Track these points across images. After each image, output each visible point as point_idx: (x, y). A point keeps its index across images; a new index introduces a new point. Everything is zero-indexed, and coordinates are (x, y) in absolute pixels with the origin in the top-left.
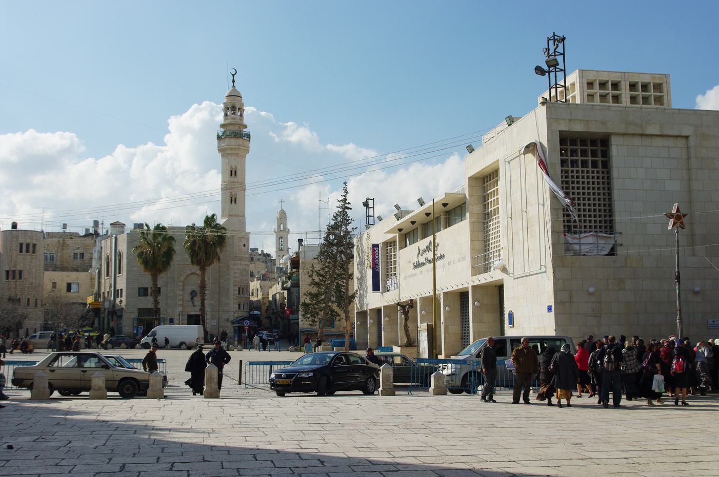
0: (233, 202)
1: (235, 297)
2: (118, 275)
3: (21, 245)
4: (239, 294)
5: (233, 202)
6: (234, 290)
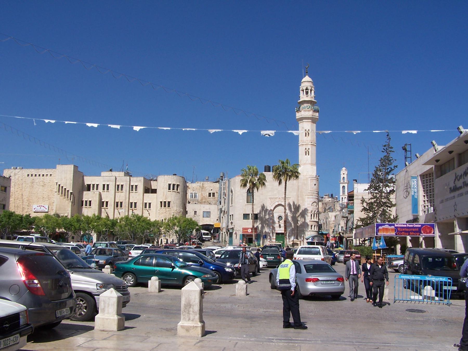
0: (307, 154)
2: (230, 205)
3: (170, 185)
5: (307, 154)
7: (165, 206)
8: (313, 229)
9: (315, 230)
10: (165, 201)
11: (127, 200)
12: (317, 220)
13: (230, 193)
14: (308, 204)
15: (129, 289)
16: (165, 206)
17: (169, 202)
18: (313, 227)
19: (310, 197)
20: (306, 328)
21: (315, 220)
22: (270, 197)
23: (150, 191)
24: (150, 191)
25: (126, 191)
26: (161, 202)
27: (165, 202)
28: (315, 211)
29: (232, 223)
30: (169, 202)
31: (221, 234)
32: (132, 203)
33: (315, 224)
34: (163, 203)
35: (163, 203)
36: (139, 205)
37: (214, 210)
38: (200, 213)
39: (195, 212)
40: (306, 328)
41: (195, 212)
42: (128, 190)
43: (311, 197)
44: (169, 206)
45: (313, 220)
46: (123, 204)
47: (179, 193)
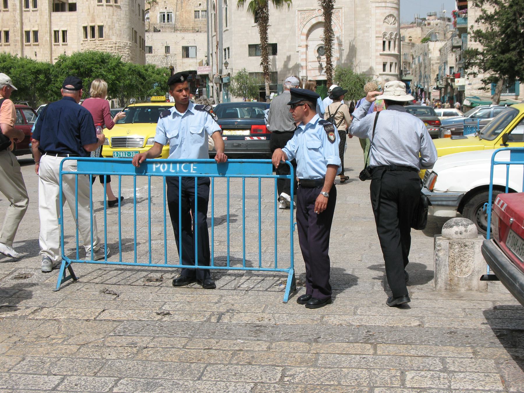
1: (378, 54)
2: (224, 29)
4: (384, 50)
6: (377, 45)
7: (93, 36)
8: (387, 71)
9: (393, 72)
10: (93, 24)
11: (18, 26)
12: (396, 52)
13: (224, 6)
14: (377, 20)
15: (459, 82)
16: (93, 36)
17: (101, 28)
18: (388, 67)
19: (380, 5)
20: (482, 80)
21: (392, 52)
22: (300, 9)
23: (67, 7)
24: (67, 7)
25: (14, 10)
26: (85, 28)
27: (93, 28)
28: (391, 34)
29: (226, 64)
30: (101, 28)
31: (211, 89)
32: (28, 33)
33: (394, 60)
34: (89, 30)
35: (89, 30)
36: (45, 37)
37: (199, 41)
38: (177, 50)
39: (167, 49)
40: (482, 80)
41: (167, 49)
42: (18, 7)
43: (383, 5)
44: (101, 35)
45: (387, 52)
46: (11, 35)
47: (119, 7)
